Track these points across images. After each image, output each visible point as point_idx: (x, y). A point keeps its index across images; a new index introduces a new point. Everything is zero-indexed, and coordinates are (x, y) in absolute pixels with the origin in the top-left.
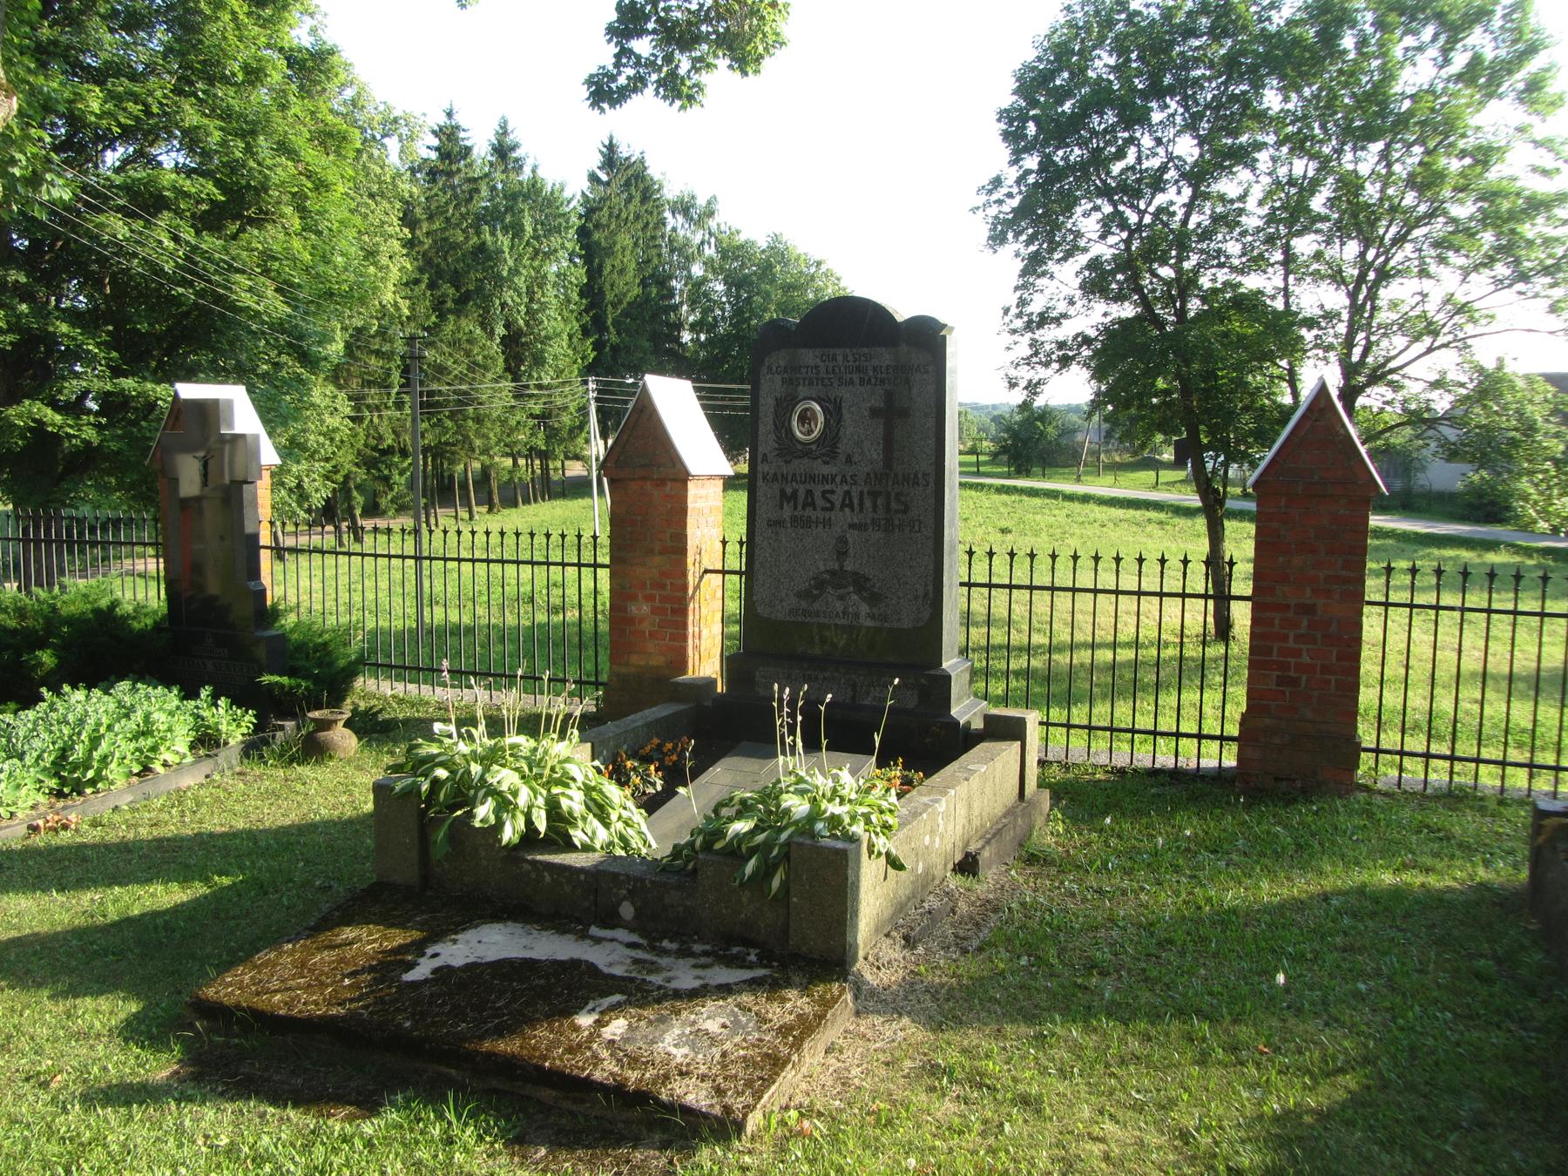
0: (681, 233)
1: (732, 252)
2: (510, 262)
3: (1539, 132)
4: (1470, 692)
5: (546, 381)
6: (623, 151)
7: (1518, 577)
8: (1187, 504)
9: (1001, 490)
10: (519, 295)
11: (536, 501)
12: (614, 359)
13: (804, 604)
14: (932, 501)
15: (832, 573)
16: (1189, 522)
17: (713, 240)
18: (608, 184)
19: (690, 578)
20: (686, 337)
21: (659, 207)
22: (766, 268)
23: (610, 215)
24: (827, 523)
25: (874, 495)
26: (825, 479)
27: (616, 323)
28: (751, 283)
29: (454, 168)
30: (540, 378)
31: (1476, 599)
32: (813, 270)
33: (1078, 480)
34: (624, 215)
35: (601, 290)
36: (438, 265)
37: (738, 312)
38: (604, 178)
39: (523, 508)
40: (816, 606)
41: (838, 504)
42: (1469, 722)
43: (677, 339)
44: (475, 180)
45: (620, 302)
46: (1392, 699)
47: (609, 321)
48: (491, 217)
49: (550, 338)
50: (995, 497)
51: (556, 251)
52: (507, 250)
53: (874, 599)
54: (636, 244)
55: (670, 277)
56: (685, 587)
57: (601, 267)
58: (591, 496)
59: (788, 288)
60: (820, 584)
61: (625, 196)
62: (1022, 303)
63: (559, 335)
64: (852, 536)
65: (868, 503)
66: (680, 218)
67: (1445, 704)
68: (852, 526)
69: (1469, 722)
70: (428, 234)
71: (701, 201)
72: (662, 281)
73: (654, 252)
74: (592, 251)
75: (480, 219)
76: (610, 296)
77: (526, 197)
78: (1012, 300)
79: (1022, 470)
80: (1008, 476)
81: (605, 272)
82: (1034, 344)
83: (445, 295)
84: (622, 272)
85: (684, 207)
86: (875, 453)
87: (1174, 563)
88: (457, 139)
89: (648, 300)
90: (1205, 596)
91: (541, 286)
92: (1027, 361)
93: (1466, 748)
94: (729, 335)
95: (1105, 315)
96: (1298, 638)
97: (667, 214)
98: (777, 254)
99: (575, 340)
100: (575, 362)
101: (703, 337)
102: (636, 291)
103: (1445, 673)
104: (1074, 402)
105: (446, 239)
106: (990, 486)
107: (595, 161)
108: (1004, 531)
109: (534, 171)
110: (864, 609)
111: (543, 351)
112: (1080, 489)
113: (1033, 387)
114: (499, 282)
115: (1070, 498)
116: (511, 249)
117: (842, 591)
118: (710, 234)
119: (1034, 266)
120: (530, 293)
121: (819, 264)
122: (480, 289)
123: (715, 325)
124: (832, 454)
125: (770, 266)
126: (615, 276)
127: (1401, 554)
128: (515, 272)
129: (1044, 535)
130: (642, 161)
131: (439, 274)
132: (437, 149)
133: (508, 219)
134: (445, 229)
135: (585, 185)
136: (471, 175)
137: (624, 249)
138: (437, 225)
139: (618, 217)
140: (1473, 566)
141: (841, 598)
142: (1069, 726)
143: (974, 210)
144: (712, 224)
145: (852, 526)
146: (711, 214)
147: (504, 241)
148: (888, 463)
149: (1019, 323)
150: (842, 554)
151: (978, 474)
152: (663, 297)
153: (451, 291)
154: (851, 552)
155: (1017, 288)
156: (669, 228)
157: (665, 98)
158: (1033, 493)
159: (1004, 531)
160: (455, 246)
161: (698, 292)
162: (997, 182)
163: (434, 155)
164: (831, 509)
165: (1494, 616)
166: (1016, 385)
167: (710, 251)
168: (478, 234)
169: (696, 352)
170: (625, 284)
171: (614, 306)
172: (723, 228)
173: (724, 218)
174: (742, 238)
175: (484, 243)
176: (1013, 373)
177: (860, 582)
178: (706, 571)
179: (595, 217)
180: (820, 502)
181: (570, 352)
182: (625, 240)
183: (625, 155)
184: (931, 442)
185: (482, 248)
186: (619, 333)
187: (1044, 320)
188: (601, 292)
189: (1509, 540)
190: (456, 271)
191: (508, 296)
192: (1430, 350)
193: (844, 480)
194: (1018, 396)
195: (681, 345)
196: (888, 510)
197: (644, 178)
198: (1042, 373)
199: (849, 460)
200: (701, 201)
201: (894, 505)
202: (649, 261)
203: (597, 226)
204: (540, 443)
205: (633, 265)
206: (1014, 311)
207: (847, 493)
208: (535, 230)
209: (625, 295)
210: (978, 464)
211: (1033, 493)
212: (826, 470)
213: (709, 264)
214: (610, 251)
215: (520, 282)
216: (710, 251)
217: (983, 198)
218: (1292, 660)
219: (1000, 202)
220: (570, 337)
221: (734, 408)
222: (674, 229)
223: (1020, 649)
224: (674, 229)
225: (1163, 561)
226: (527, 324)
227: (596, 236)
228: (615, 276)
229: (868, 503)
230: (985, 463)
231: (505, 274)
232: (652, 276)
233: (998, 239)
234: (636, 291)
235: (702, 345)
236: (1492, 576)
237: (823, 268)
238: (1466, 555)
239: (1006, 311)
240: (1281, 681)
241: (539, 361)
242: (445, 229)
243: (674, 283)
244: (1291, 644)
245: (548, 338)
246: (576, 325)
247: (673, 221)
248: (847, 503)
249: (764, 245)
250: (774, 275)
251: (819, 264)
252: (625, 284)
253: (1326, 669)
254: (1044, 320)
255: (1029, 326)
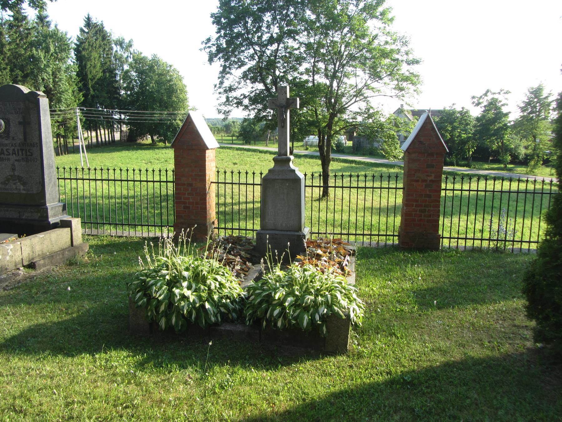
0: (119, 53)
1: (139, 61)
2: (45, 62)
3: (388, 29)
4: (361, 214)
5: (63, 108)
6: (94, 21)
7: (397, 177)
8: (300, 154)
9: (238, 149)
10: (49, 75)
11: (62, 154)
12: (93, 100)
13: (3, 186)
14: (39, 152)
15: (11, 176)
16: (299, 160)
17: (132, 56)
18: (88, 33)
19: (207, 186)
20: (123, 92)
21: (109, 42)
22: (151, 68)
23: (89, 45)
24: (9, 159)
25: (22, 150)
26: (6, 145)
27: (92, 87)
28: (146, 73)
29: (20, 24)
30: (60, 107)
31: (385, 184)
32: (169, 68)
33: (267, 145)
34: (94, 45)
35: (86, 73)
36: (14, 63)
37: (142, 83)
38: (86, 30)
39: (61, 156)
40: (7, 187)
41: (11, 153)
42: (360, 224)
43: (119, 94)
44: (29, 29)
45: (94, 78)
46: (330, 216)
47: (90, 86)
48: (36, 45)
49: (63, 92)
50: (236, 152)
51: (64, 58)
52: (43, 57)
53: (24, 184)
54: (100, 57)
55: (115, 70)
56: (205, 189)
57: (86, 65)
58: (79, 152)
59: (160, 75)
60: (8, 180)
61: (95, 38)
62: (221, 83)
63: (67, 91)
64: (16, 163)
65: (20, 153)
66: (118, 47)
67: (353, 219)
68: (16, 160)
69: (360, 224)
70: (9, 50)
71: (127, 41)
72: (112, 72)
73: (108, 60)
74: (80, 58)
75: (32, 44)
76: (90, 76)
77: (51, 37)
78: (217, 82)
79: (248, 142)
80: (243, 144)
81: (88, 67)
82: (228, 98)
83: (17, 74)
84: (95, 67)
85: (120, 43)
86: (21, 137)
87: (144, 171)
88: (21, 13)
89: (105, 78)
90: (320, 187)
91: (59, 72)
92: (224, 104)
93: (353, 231)
94: (138, 92)
95: (252, 88)
96: (189, 194)
97: (113, 45)
98: (155, 62)
99: (75, 93)
100: (75, 101)
101: (129, 93)
102: (101, 74)
103: (353, 207)
104: (240, 117)
105: (17, 52)
106: (234, 148)
107: (82, 24)
108: (235, 164)
109: (56, 27)
110: (22, 187)
111: (60, 97)
112: (265, 149)
113: (227, 113)
114: (40, 70)
115: (261, 152)
116: (45, 57)
117: (15, 182)
118: (131, 54)
119: (225, 71)
120: (53, 74)
121: (171, 66)
122: (32, 73)
123: (133, 88)
124: (8, 137)
125: (153, 67)
126: (92, 68)
127: (362, 169)
128: (47, 66)
129: (248, 165)
130: (102, 25)
131: (15, 66)
132: (13, 16)
133: (44, 45)
134: (16, 48)
135: (79, 33)
136: (27, 27)
137: (95, 58)
138: (13, 46)
139: (92, 46)
140: (384, 173)
141: (15, 184)
142: (239, 229)
143: (201, 50)
144: (131, 50)
145: (16, 160)
146: (131, 46)
147: (42, 54)
148: (25, 138)
149: (221, 90)
150: (14, 170)
151: (233, 144)
152: (112, 77)
153: (20, 73)
154: (17, 169)
155: (219, 78)
156: (114, 50)
157: (33, 7)
158: (248, 150)
159: (235, 164)
160: (21, 55)
161: (126, 76)
162: (209, 40)
163: (12, 19)
164: (9, 155)
165: (382, 190)
166: (221, 112)
167: (130, 60)
168: (31, 51)
169: (127, 98)
170: (95, 71)
171: (92, 80)
172: (136, 51)
173: (135, 48)
174: (142, 55)
175: (33, 54)
176: (220, 108)
177: (20, 179)
178: (212, 182)
179: (83, 45)
180: (6, 153)
181: (73, 98)
182: (95, 55)
183: (94, 22)
184: (38, 133)
185: (33, 56)
186: (94, 90)
187: (231, 89)
188: (86, 75)
189: (399, 165)
190: (22, 65)
191: (45, 76)
192: (355, 101)
193: (12, 146)
194: (222, 116)
195: (120, 95)
196: (26, 155)
197: (103, 31)
198: (230, 108)
199: (13, 139)
200: (127, 41)
201: (28, 153)
202: (106, 63)
203: (84, 49)
204: (62, 133)
205: (99, 64)
206: (218, 86)
207: (14, 150)
208: (55, 50)
209: (96, 76)
210: (232, 140)
211: (248, 150)
212: (6, 142)
213: (130, 65)
214: (89, 59)
215: (49, 70)
216: (130, 60)
217: (204, 45)
218: (187, 201)
219: (209, 47)
220: (73, 92)
221: (141, 120)
222: (116, 51)
223: (222, 204)
224: (116, 51)
225: (232, 172)
226: (54, 86)
227: (83, 53)
228: (92, 68)
229: (20, 153)
230: (235, 140)
231: (42, 67)
232: (107, 69)
233: (211, 60)
234: (101, 74)
235: (128, 96)
236: (389, 177)
237: (172, 68)
238: (384, 169)
239: (215, 86)
240: (185, 208)
241: (59, 101)
242: (16, 48)
243: (117, 72)
244: (187, 196)
245: (63, 92)
246: (76, 88)
247: (115, 48)
248: (14, 153)
249: (151, 59)
250: (155, 70)
251: (171, 66)
252: (95, 71)
253: (197, 203)
254: (231, 89)
255: (226, 91)
